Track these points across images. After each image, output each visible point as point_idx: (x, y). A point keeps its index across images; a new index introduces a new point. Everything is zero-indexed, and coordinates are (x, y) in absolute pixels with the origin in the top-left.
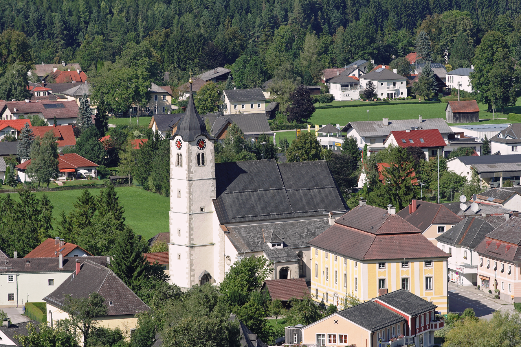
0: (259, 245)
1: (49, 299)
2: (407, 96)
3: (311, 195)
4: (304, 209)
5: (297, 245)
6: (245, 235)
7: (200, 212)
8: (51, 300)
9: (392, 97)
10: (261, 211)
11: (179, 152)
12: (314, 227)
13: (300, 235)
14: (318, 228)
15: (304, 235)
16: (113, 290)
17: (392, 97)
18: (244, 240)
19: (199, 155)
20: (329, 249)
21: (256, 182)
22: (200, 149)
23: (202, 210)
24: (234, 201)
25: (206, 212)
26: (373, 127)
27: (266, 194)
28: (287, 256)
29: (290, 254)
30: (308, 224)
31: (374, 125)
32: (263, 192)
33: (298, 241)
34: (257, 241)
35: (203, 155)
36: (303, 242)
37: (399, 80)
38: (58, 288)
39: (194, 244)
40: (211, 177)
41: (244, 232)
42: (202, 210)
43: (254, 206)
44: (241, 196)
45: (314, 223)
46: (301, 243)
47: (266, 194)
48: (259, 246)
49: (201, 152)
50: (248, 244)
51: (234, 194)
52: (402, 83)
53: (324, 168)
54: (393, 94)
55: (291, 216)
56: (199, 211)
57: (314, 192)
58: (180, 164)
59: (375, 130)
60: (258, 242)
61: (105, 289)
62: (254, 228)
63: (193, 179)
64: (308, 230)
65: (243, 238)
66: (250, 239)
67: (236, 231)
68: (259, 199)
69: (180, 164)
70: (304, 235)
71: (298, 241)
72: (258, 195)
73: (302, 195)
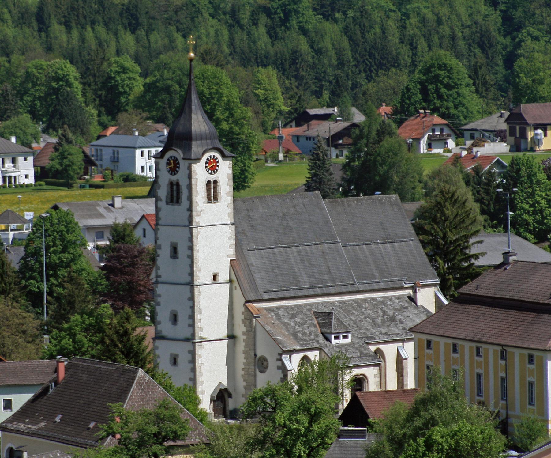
0: (312, 337)
1: (9, 426)
2: (35, 181)
3: (381, 253)
4: (374, 277)
5: (372, 337)
6: (287, 320)
7: (211, 282)
8: (22, 426)
9: (10, 182)
10: (306, 279)
11: (174, 178)
12: (391, 308)
13: (373, 321)
14: (399, 309)
15: (379, 321)
16: (148, 404)
17: (10, 182)
18: (287, 328)
19: (209, 182)
20: (470, 338)
21: (294, 230)
22: (211, 174)
23: (215, 277)
24: (265, 264)
25: (220, 281)
26: (97, 210)
27: (312, 252)
28: (361, 357)
29: (365, 352)
30: (382, 303)
31: (98, 208)
32: (307, 247)
33: (372, 331)
34: (307, 331)
35: (215, 182)
36: (381, 333)
37: (21, 154)
38: (21, 408)
39: (204, 336)
40: (229, 222)
41: (283, 315)
42: (215, 277)
43: (295, 272)
44: (274, 254)
45: (391, 300)
46: (377, 334)
47: (312, 252)
48: (312, 339)
49: (212, 178)
50: (295, 335)
51: (262, 251)
52: (26, 160)
53: (396, 208)
54: (7, 179)
55: (354, 289)
56: (210, 280)
57: (385, 248)
58: (175, 198)
59: (101, 216)
60: (310, 333)
61: (136, 402)
62: (298, 308)
63: (201, 225)
64: (384, 313)
65: (285, 325)
66: (297, 327)
67: (272, 313)
68: (302, 260)
69: (175, 198)
70: (379, 321)
71: (372, 331)
72: (299, 252)
73: (367, 253)
